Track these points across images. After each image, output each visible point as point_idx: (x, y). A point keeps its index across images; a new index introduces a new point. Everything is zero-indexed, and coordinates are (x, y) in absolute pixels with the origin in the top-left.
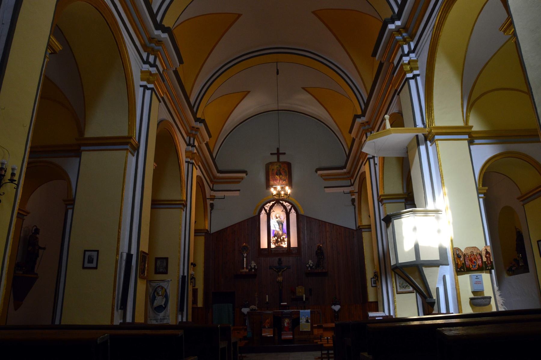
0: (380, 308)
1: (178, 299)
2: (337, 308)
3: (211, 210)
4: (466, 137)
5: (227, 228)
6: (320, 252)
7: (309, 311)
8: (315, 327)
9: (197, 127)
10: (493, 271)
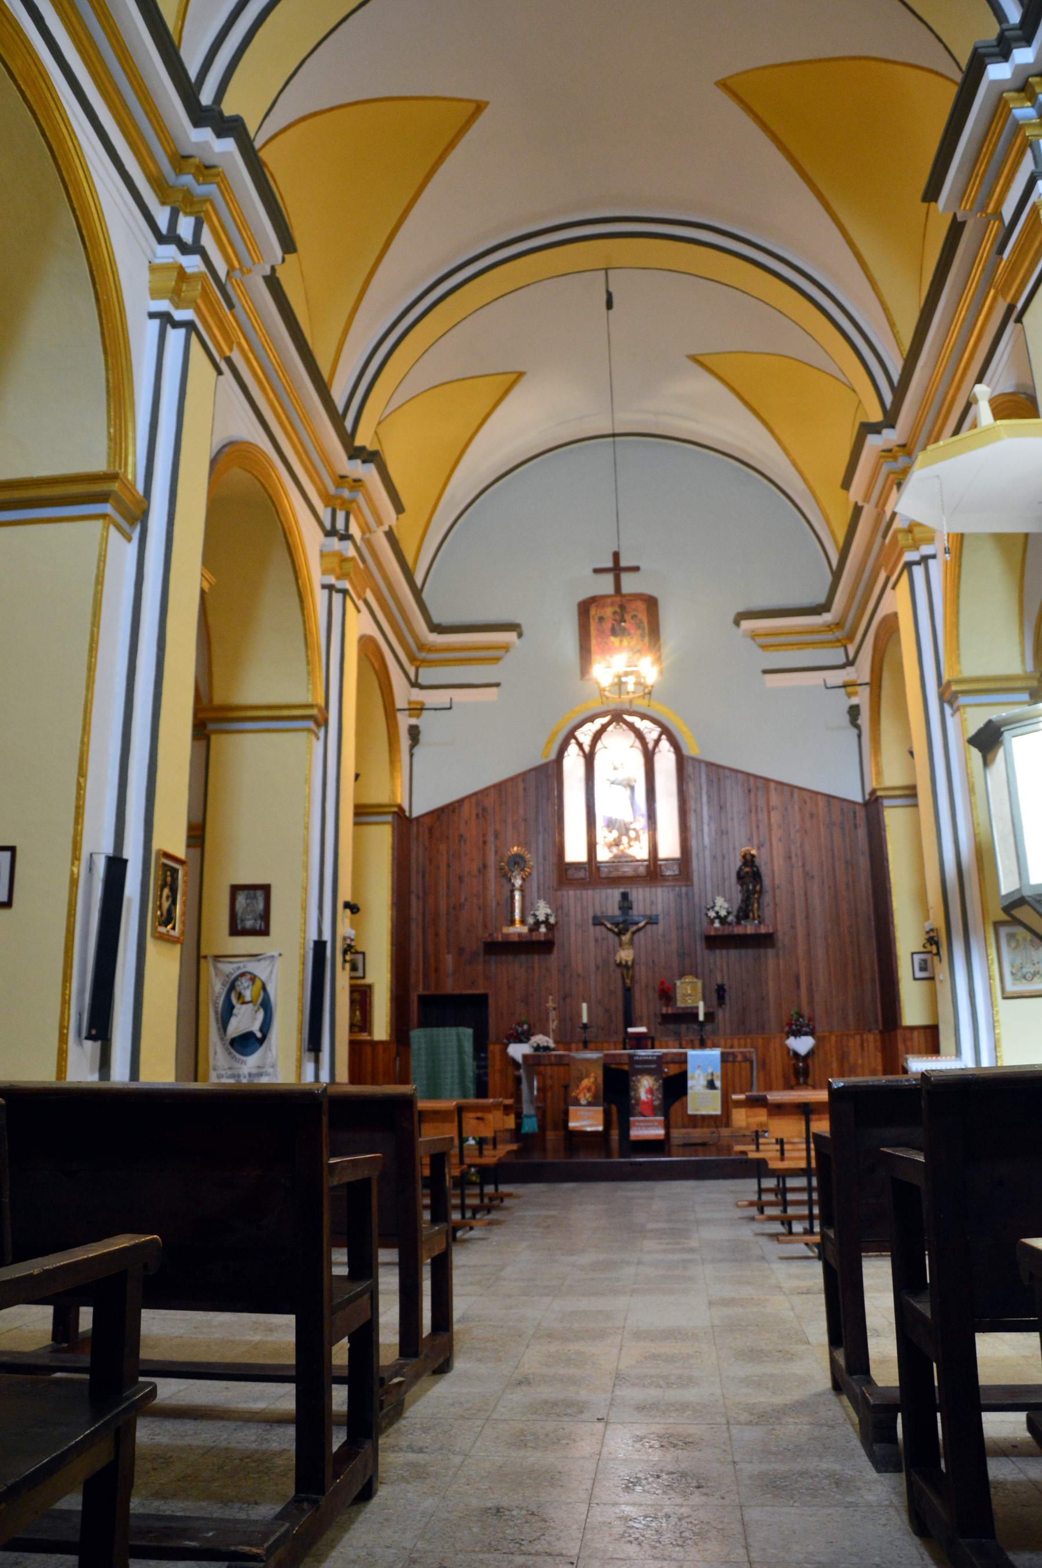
1: (302, 1012)
2: (802, 1045)
5: (460, 802)
6: (750, 874)
7: (716, 1052)
8: (739, 1104)
9: (356, 476)
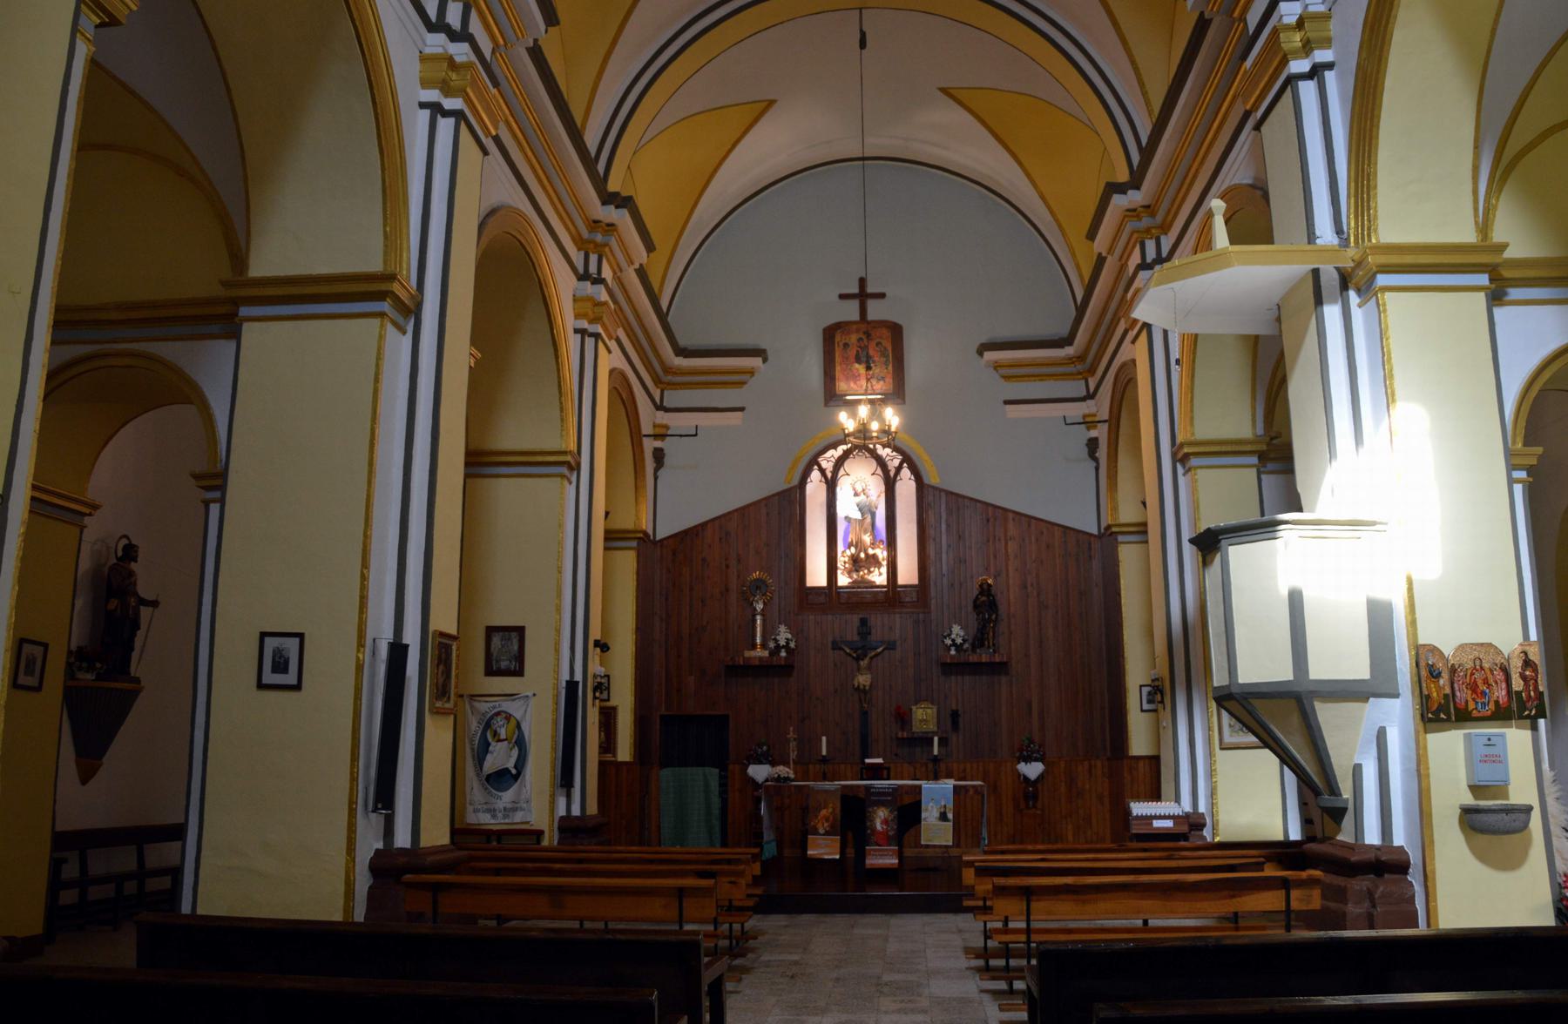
0: (1167, 787)
1: (554, 749)
2: (1033, 770)
3: (656, 470)
4: (1483, 279)
5: (703, 525)
6: (986, 603)
10: (1542, 722)
